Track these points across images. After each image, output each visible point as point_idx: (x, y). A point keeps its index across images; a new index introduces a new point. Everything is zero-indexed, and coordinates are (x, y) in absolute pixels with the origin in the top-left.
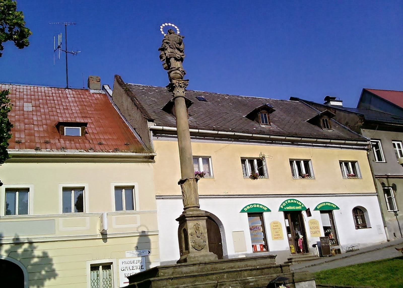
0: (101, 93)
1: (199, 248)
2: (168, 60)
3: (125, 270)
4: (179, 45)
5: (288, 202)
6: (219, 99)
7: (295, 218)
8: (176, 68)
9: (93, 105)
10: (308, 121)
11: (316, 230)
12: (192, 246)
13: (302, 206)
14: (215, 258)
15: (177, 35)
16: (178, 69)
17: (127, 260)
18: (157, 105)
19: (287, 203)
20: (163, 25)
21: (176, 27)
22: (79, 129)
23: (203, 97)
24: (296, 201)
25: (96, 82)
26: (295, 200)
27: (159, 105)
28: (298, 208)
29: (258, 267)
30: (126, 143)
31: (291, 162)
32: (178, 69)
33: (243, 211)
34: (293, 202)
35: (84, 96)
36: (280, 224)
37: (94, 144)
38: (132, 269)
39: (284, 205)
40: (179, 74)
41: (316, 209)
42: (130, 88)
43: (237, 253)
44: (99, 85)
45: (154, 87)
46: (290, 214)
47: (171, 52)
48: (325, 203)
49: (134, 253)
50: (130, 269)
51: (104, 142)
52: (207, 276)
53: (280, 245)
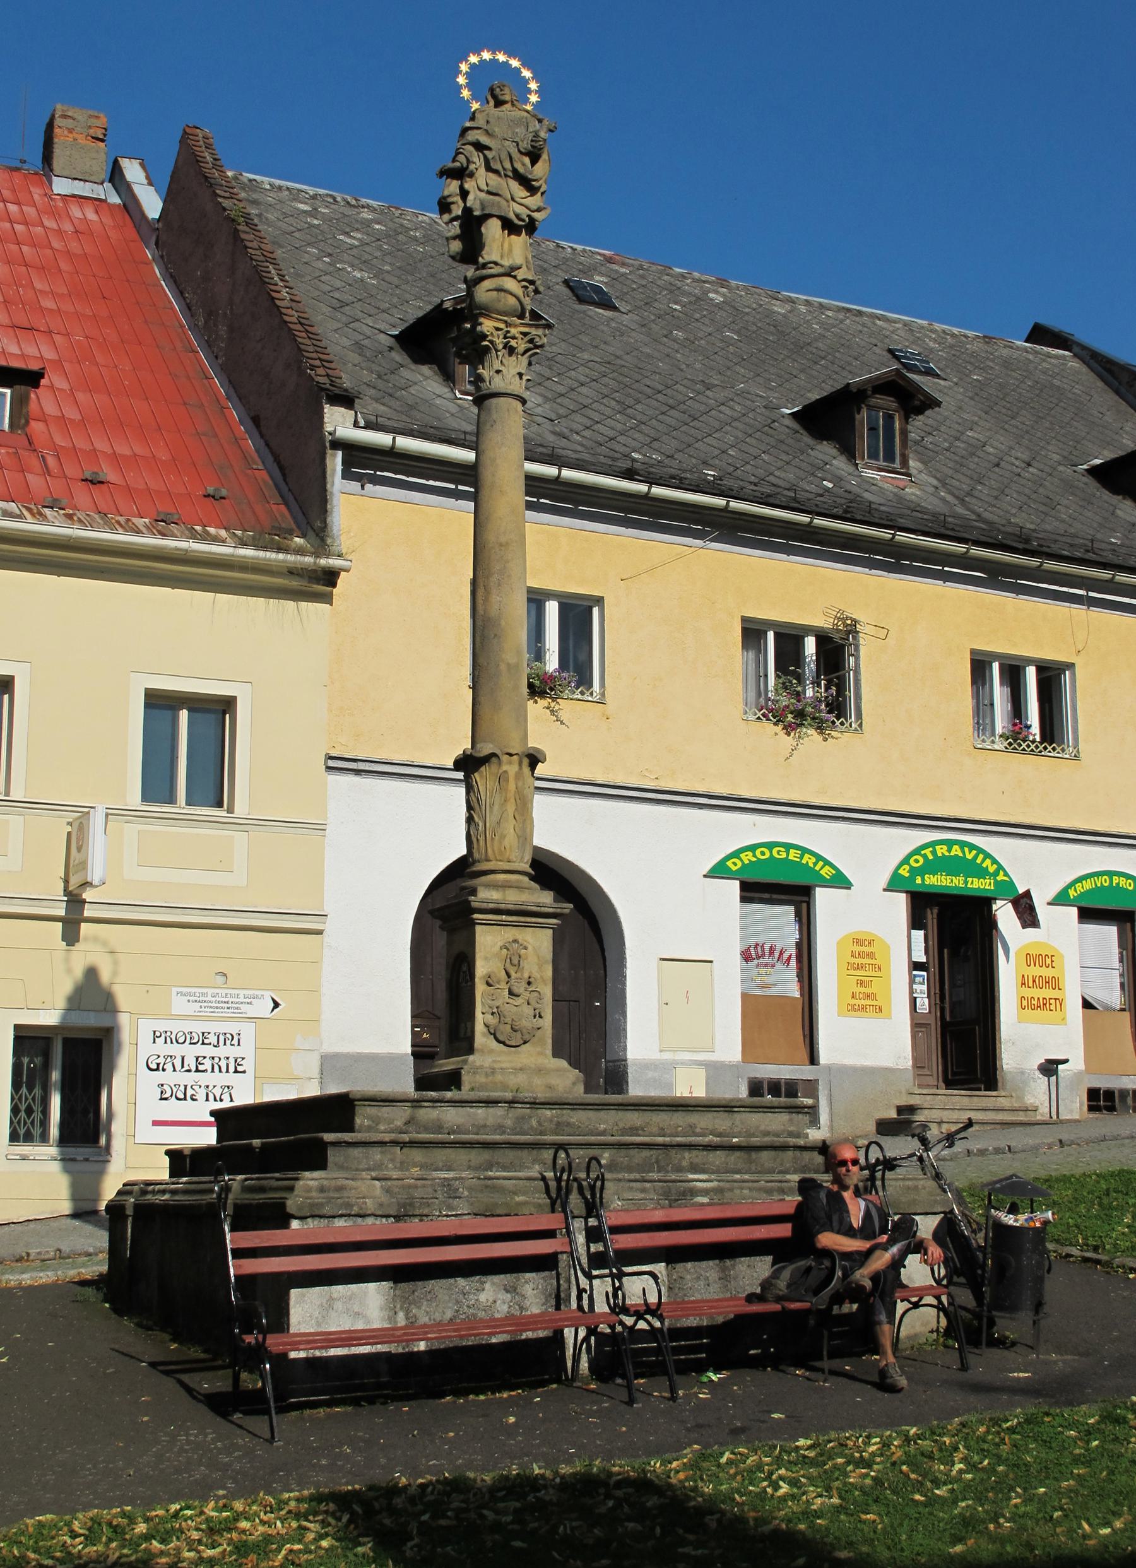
0: (105, 201)
1: (511, 1037)
2: (471, 227)
3: (164, 1070)
4: (527, 160)
5: (934, 853)
6: (676, 303)
7: (958, 931)
8: (502, 266)
9: (64, 266)
10: (1094, 472)
11: (1047, 993)
12: (486, 1026)
13: (1001, 877)
14: (574, 1084)
15: (527, 111)
16: (510, 273)
17: (175, 1027)
18: (373, 311)
19: (931, 857)
20: (473, 59)
21: (526, 74)
22: (4, 395)
23: (598, 280)
24: (974, 852)
25: (82, 140)
26: (972, 847)
27: (384, 311)
28: (978, 885)
29: (734, 1140)
30: (210, 490)
31: (979, 666)
32: (510, 273)
33: (718, 872)
34: (961, 855)
35: (24, 208)
36: (886, 947)
37: (66, 477)
38: (194, 1069)
39: (917, 865)
40: (515, 296)
41: (1060, 900)
42: (255, 202)
43: (668, 1056)
44: (98, 159)
45: (368, 206)
46: (935, 911)
47: (489, 193)
48: (1110, 874)
49: (209, 998)
50: (186, 1068)
51: (109, 473)
52: (535, 1152)
53: (873, 1037)
